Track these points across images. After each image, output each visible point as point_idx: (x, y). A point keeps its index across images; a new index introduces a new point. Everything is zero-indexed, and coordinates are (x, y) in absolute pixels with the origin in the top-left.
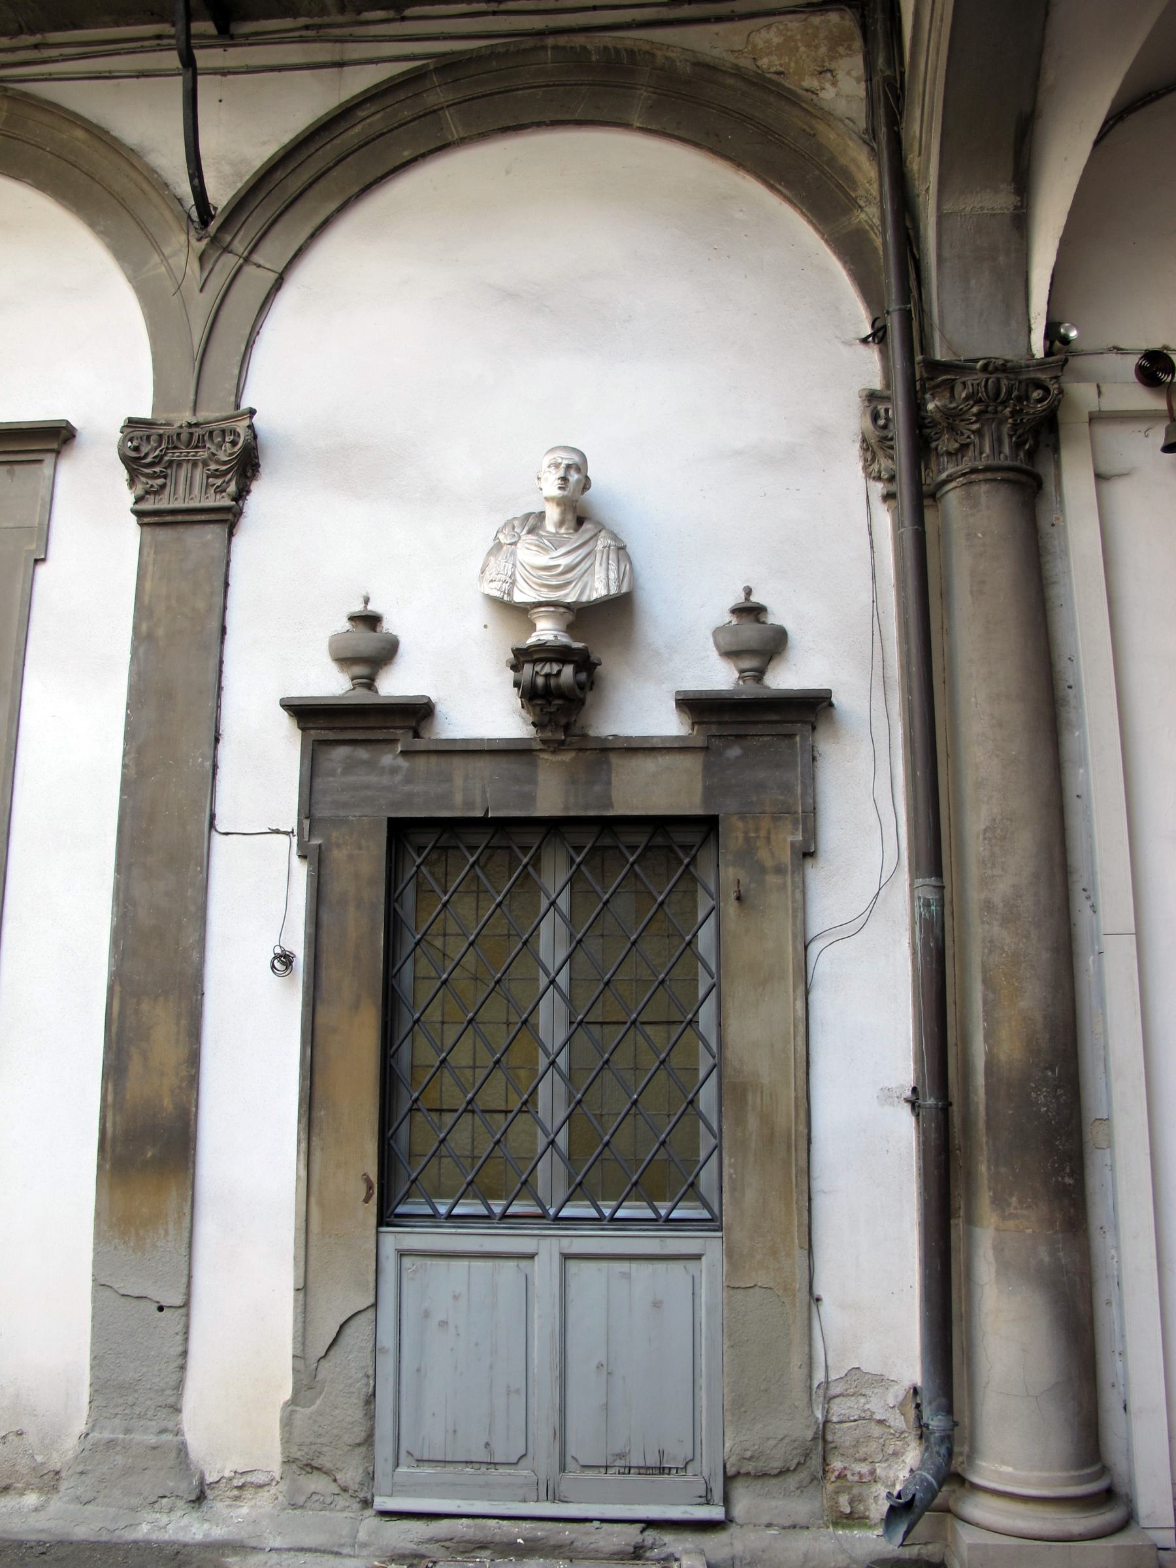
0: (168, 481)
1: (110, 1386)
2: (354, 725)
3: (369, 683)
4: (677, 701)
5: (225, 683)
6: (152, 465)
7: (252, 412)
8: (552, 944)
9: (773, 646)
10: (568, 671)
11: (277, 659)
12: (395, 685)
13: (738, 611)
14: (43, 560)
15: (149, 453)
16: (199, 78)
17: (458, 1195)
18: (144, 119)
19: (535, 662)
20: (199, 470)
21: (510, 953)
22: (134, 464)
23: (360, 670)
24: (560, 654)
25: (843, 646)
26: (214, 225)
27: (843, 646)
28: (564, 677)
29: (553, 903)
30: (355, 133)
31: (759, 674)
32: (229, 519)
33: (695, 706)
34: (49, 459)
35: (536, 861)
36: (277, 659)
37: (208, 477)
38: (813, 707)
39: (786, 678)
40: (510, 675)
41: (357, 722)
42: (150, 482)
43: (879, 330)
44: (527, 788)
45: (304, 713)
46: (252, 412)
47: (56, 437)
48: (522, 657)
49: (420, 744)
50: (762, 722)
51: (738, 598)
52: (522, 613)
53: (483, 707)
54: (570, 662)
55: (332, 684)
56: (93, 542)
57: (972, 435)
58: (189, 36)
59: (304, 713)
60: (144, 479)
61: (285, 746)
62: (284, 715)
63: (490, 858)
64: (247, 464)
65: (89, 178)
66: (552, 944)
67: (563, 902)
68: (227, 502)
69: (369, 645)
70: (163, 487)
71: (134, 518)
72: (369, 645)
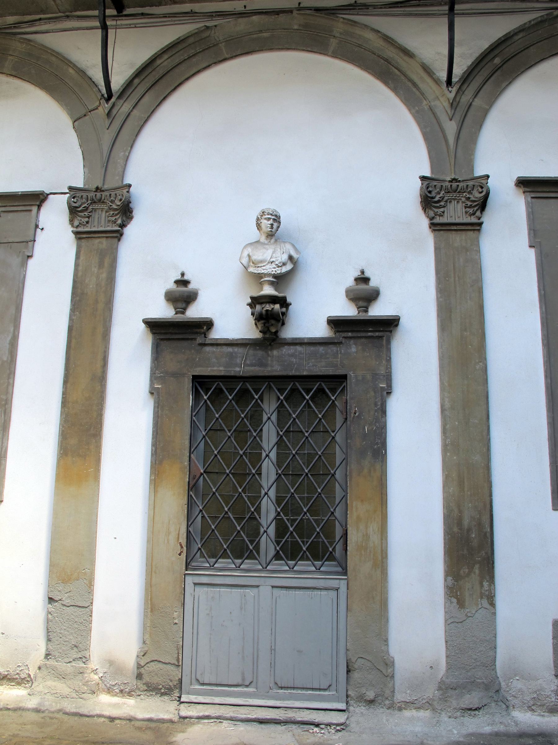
0: (90, 220)
2: (177, 331)
4: (328, 320)
6: (81, 211)
7: (130, 186)
8: (270, 435)
10: (277, 306)
11: (139, 300)
12: (195, 312)
15: (81, 205)
16: (109, 30)
17: (218, 557)
18: (79, 46)
19: (261, 303)
20: (104, 214)
21: (247, 443)
22: (73, 211)
23: (361, 303)
24: (273, 300)
25: (411, 296)
26: (113, 100)
27: (411, 296)
28: (271, 313)
29: (269, 418)
30: (180, 47)
32: (118, 235)
33: (336, 323)
35: (261, 398)
36: (139, 300)
37: (108, 217)
38: (390, 324)
39: (378, 310)
40: (249, 310)
41: (177, 331)
42: (82, 219)
44: (267, 544)
45: (154, 326)
46: (130, 186)
47: (38, 199)
48: (255, 301)
50: (367, 330)
51: (357, 274)
52: (258, 278)
54: (277, 303)
58: (105, 16)
59: (154, 326)
60: (80, 218)
62: (143, 325)
63: (261, 262)
64: (126, 211)
65: (53, 76)
66: (270, 435)
67: (274, 417)
68: (117, 228)
69: (182, 294)
70: (87, 222)
71: (73, 236)
72: (182, 294)
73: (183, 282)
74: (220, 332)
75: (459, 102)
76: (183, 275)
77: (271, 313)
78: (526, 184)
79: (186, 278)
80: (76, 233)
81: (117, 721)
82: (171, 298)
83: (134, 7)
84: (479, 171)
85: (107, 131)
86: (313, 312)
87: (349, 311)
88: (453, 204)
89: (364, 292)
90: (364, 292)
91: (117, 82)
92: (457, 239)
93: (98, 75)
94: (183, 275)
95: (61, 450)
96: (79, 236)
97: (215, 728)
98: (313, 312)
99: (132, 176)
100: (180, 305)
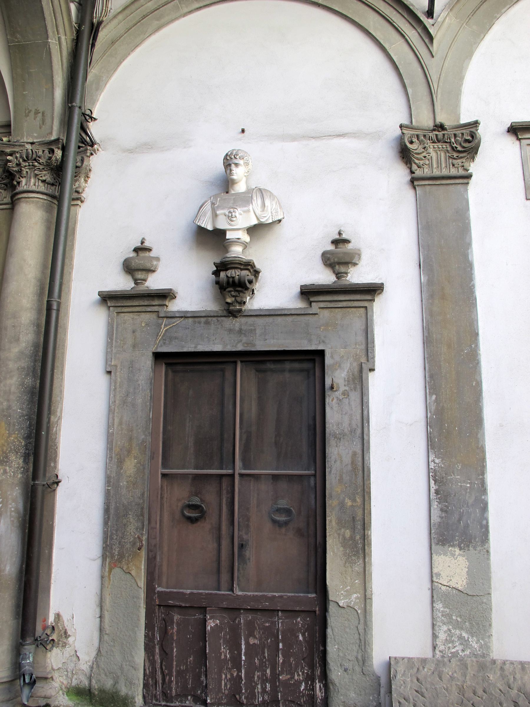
10: (244, 273)
12: (155, 282)
25: (390, 256)
27: (390, 256)
33: (308, 293)
38: (373, 290)
39: (357, 276)
45: (108, 299)
55: (122, 283)
69: (139, 262)
72: (139, 262)
73: (339, 242)
74: (181, 304)
76: (340, 234)
77: (233, 281)
78: (516, 130)
79: (344, 236)
82: (129, 268)
83: (44, 19)
86: (281, 278)
88: (437, 154)
89: (339, 255)
90: (339, 255)
92: (439, 192)
94: (340, 234)
95: (108, 443)
98: (281, 278)
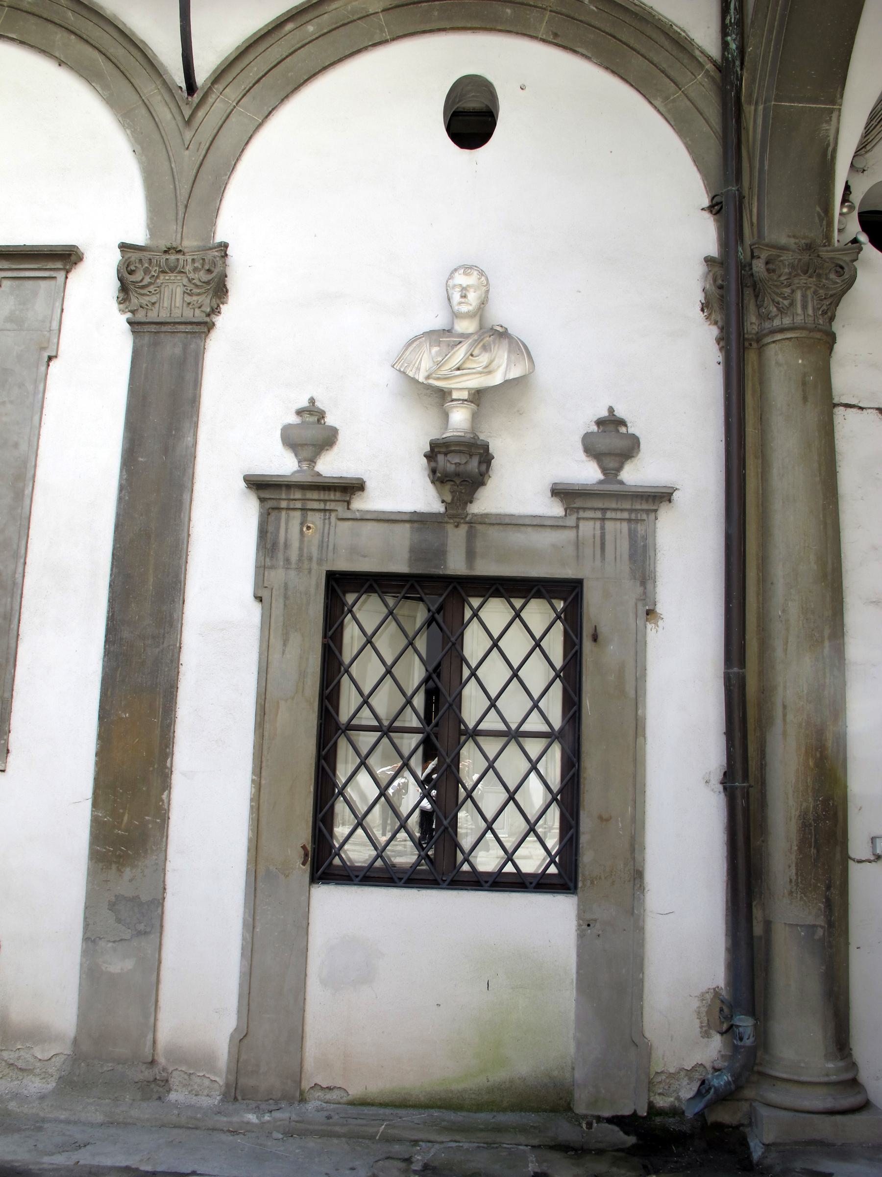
1: (94, 979)
3: (611, 472)
5: (45, 405)
9: (630, 448)
12: (331, 466)
13: (600, 423)
14: (56, 357)
15: (135, 274)
20: (176, 293)
22: (126, 289)
27: (683, 453)
28: (459, 467)
31: (312, 461)
32: (204, 327)
33: (562, 493)
34: (60, 275)
36: (237, 435)
38: (660, 497)
39: (633, 475)
43: (717, 204)
45: (261, 486)
46: (225, 246)
47: (66, 258)
49: (348, 515)
53: (401, 486)
55: (283, 464)
56: (93, 346)
57: (762, 298)
59: (261, 486)
61: (246, 514)
69: (312, 432)
72: (312, 432)
74: (372, 501)
75: (154, 1042)
77: (459, 467)
80: (130, 323)
81: (53, 1060)
82: (291, 440)
84: (219, 238)
85: (187, 152)
86: (523, 484)
87: (587, 473)
91: (201, 76)
93: (169, 55)
96: (137, 328)
97: (231, 1138)
99: (228, 227)
100: (307, 453)
